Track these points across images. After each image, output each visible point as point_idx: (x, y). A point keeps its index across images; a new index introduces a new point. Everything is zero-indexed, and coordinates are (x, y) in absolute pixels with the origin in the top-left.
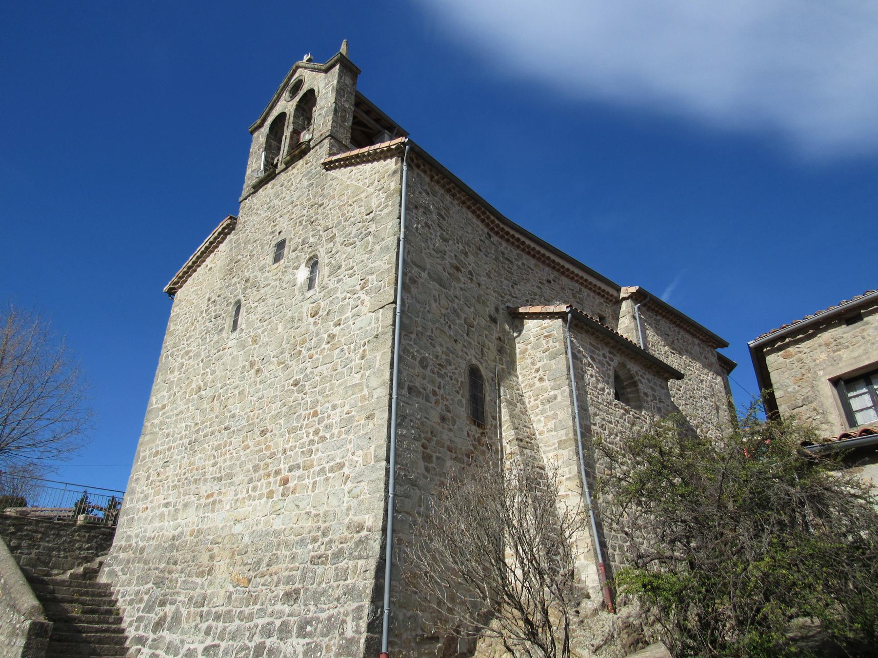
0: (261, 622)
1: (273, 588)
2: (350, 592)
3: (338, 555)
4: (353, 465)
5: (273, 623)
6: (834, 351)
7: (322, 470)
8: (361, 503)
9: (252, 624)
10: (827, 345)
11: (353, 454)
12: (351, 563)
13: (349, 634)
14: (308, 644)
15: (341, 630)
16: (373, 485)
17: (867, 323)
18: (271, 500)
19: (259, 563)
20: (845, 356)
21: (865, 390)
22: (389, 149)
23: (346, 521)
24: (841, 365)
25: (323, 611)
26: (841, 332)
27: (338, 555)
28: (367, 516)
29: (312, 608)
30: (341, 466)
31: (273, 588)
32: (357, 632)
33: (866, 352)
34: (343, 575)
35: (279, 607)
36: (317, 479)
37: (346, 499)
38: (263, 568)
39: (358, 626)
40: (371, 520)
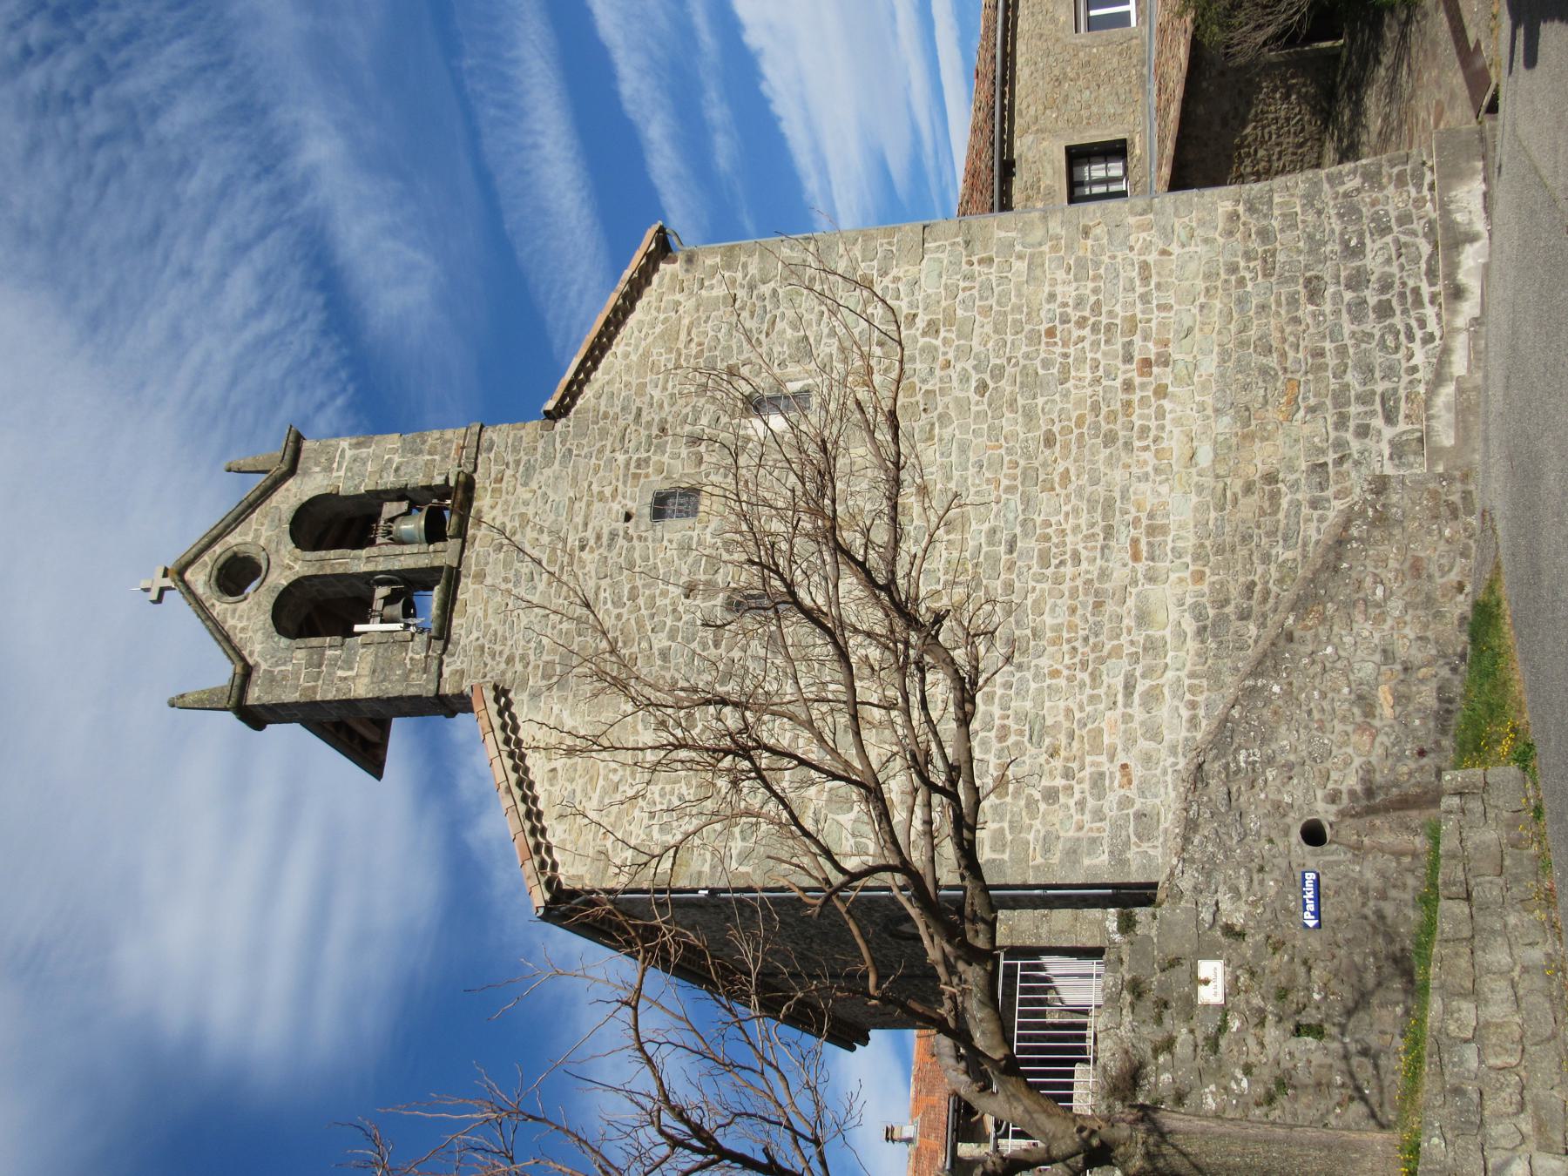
0: (1348, 327)
1: (1303, 327)
2: (1310, 199)
3: (1265, 235)
4: (1147, 247)
5: (1349, 305)
6: (1038, 192)
7: (1145, 299)
8: (1202, 223)
9: (1350, 342)
10: (1028, 198)
11: (1131, 249)
12: (1276, 212)
13: (1357, 182)
14: (1372, 234)
15: (1355, 193)
16: (1182, 209)
17: (1020, 156)
18: (1170, 389)
19: (1264, 371)
20: (1048, 182)
21: (943, 892)
22: (648, 255)
23: (1221, 240)
24: (1057, 188)
25: (1332, 231)
26: (1017, 184)
27: (1265, 235)
28: (1220, 210)
29: (1329, 248)
30: (1145, 266)
31: (1303, 327)
32: (1354, 172)
33: (1052, 162)
34: (1290, 221)
35: (1328, 308)
36: (1155, 302)
37: (1192, 249)
38: (1273, 361)
39: (1348, 174)
40: (1226, 203)
